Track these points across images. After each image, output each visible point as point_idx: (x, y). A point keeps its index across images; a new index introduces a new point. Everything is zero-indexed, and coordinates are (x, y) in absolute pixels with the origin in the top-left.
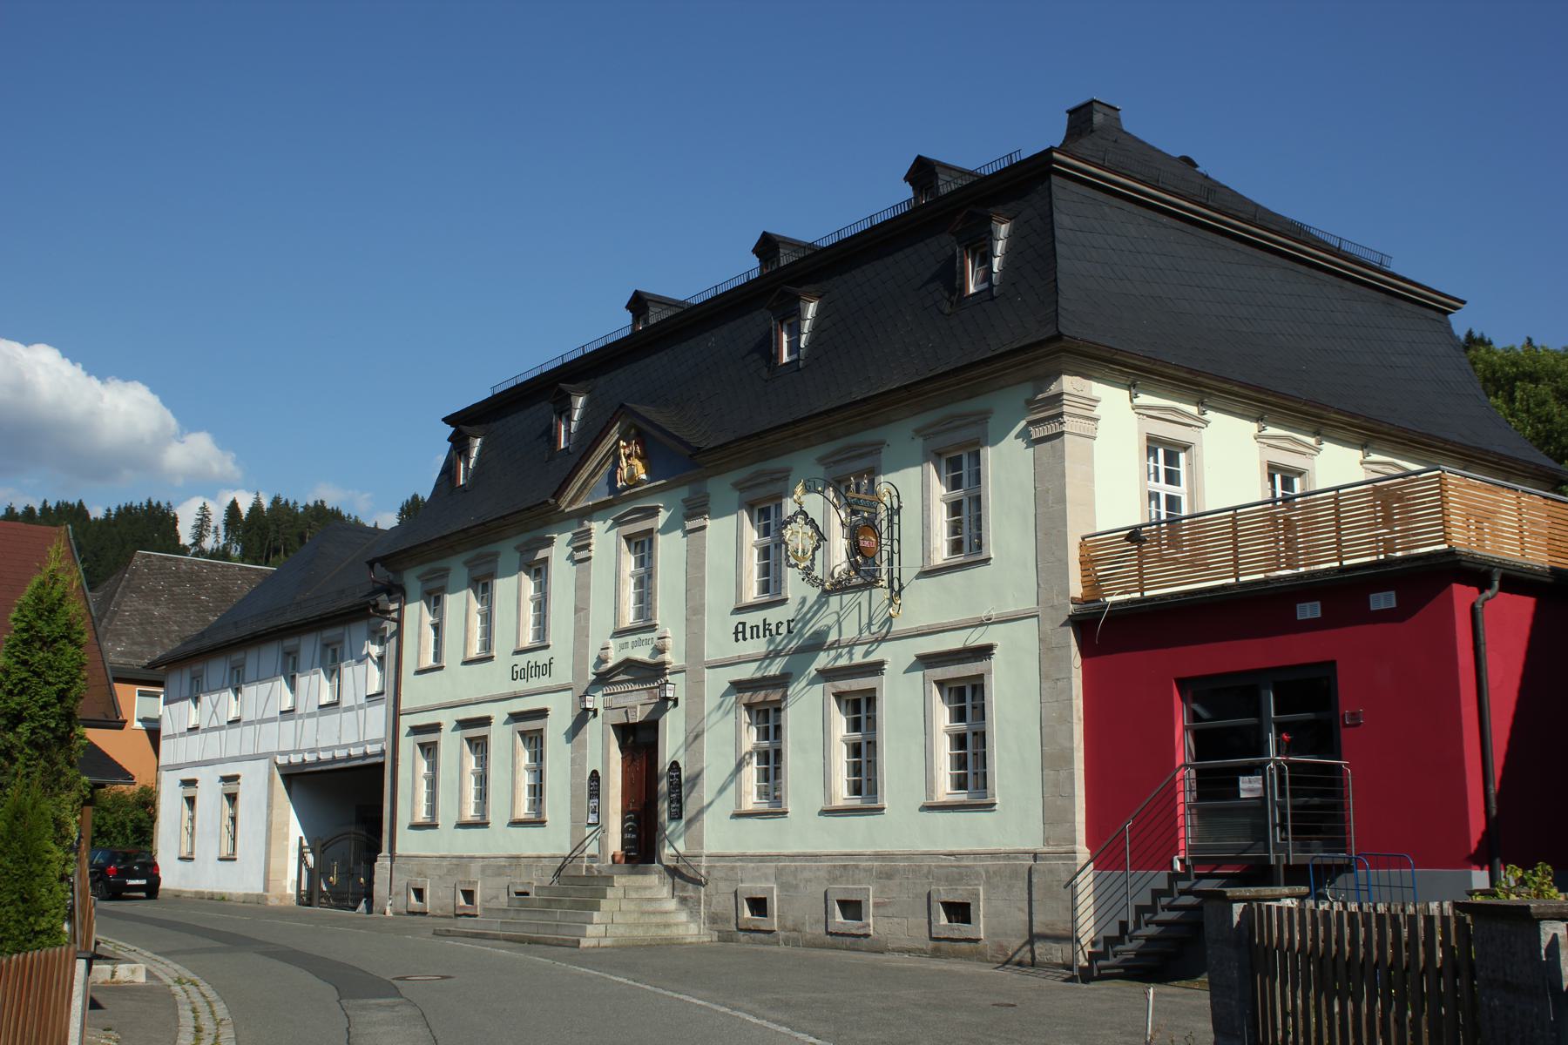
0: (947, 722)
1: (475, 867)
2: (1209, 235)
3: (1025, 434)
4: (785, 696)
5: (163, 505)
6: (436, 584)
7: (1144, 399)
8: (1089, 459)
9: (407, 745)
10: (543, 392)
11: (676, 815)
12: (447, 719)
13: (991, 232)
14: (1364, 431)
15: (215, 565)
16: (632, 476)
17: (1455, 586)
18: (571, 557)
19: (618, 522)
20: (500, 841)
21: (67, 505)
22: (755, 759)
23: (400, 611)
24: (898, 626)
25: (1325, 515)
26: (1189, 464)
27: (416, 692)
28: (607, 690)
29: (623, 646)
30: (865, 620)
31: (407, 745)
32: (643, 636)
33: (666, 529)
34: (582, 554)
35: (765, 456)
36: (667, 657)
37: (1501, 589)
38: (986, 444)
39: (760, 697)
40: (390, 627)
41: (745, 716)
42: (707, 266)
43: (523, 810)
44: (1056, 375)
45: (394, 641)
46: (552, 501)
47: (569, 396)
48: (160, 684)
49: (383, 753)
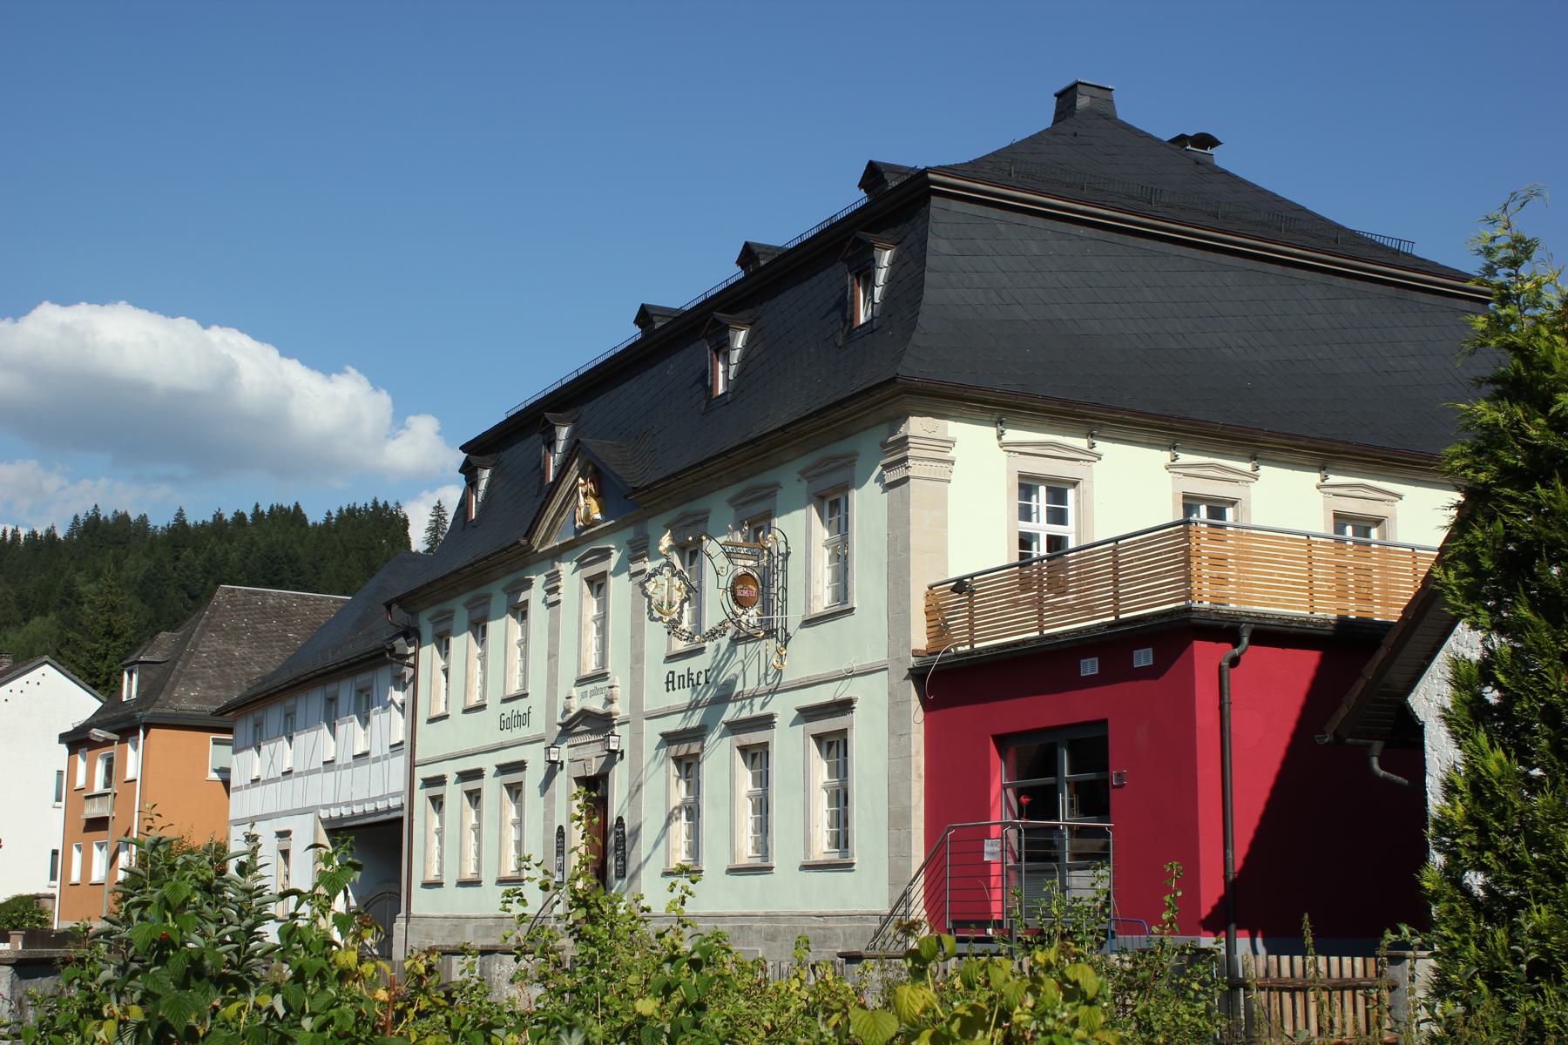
0: (826, 778)
1: (470, 927)
2: (1142, 242)
3: (880, 478)
4: (702, 748)
5: (391, 505)
6: (442, 628)
7: (1012, 435)
8: (942, 503)
9: (421, 796)
10: (528, 425)
11: (621, 874)
12: (488, 763)
13: (873, 260)
14: (1320, 451)
15: (307, 599)
16: (588, 515)
17: (1196, 643)
18: (545, 600)
19: (581, 564)
20: (790, 893)
21: (281, 508)
22: (684, 814)
23: (416, 654)
24: (788, 678)
25: (1105, 567)
26: (1078, 501)
27: (431, 742)
28: (571, 741)
29: (584, 695)
30: (763, 671)
31: (421, 796)
32: (599, 685)
33: (616, 573)
34: (553, 598)
35: (690, 498)
36: (615, 708)
37: (1252, 642)
39: (683, 749)
40: (409, 672)
41: (673, 767)
42: (696, 273)
43: (746, 853)
44: (902, 418)
45: (411, 687)
46: (523, 541)
47: (553, 427)
48: (229, 731)
49: (401, 808)
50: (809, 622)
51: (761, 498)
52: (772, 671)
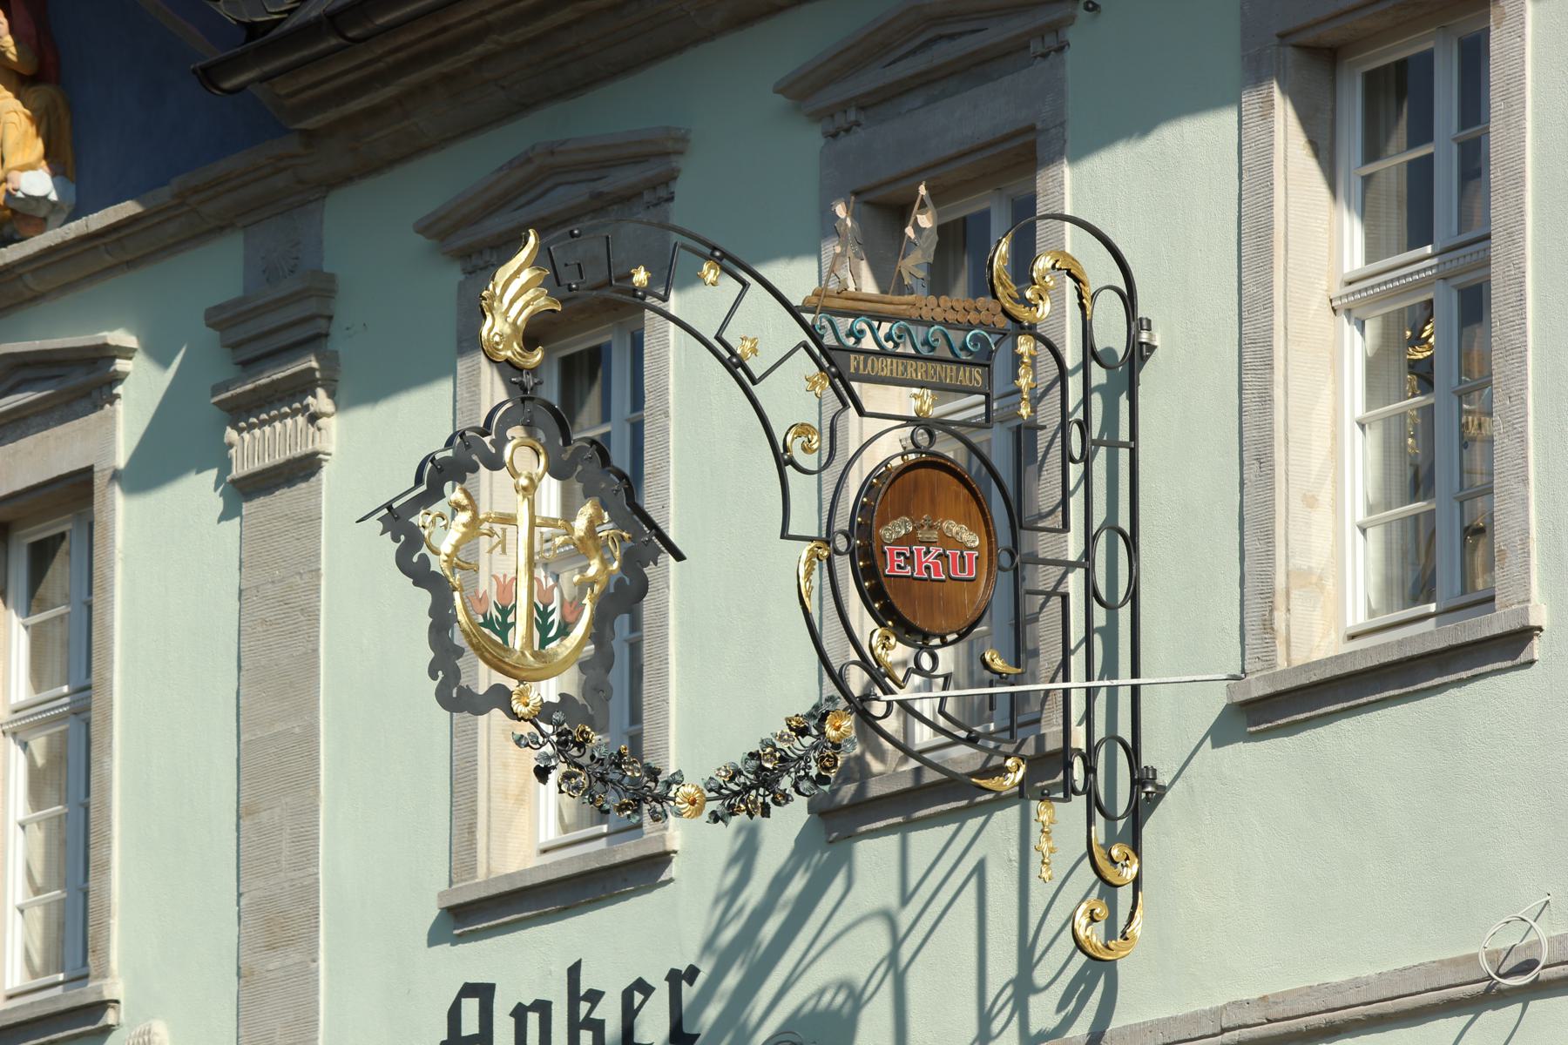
30: (1003, 968)
33: (152, 468)
38: (1054, 158)
50: (1266, 711)
51: (977, 69)
52: (1057, 964)
